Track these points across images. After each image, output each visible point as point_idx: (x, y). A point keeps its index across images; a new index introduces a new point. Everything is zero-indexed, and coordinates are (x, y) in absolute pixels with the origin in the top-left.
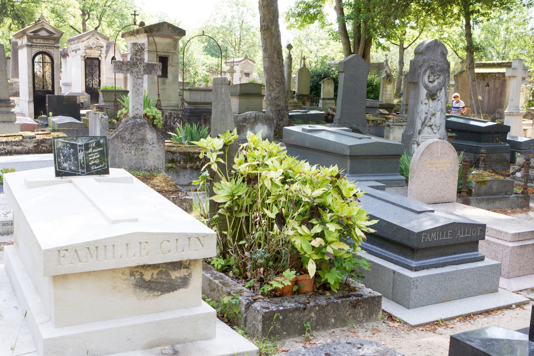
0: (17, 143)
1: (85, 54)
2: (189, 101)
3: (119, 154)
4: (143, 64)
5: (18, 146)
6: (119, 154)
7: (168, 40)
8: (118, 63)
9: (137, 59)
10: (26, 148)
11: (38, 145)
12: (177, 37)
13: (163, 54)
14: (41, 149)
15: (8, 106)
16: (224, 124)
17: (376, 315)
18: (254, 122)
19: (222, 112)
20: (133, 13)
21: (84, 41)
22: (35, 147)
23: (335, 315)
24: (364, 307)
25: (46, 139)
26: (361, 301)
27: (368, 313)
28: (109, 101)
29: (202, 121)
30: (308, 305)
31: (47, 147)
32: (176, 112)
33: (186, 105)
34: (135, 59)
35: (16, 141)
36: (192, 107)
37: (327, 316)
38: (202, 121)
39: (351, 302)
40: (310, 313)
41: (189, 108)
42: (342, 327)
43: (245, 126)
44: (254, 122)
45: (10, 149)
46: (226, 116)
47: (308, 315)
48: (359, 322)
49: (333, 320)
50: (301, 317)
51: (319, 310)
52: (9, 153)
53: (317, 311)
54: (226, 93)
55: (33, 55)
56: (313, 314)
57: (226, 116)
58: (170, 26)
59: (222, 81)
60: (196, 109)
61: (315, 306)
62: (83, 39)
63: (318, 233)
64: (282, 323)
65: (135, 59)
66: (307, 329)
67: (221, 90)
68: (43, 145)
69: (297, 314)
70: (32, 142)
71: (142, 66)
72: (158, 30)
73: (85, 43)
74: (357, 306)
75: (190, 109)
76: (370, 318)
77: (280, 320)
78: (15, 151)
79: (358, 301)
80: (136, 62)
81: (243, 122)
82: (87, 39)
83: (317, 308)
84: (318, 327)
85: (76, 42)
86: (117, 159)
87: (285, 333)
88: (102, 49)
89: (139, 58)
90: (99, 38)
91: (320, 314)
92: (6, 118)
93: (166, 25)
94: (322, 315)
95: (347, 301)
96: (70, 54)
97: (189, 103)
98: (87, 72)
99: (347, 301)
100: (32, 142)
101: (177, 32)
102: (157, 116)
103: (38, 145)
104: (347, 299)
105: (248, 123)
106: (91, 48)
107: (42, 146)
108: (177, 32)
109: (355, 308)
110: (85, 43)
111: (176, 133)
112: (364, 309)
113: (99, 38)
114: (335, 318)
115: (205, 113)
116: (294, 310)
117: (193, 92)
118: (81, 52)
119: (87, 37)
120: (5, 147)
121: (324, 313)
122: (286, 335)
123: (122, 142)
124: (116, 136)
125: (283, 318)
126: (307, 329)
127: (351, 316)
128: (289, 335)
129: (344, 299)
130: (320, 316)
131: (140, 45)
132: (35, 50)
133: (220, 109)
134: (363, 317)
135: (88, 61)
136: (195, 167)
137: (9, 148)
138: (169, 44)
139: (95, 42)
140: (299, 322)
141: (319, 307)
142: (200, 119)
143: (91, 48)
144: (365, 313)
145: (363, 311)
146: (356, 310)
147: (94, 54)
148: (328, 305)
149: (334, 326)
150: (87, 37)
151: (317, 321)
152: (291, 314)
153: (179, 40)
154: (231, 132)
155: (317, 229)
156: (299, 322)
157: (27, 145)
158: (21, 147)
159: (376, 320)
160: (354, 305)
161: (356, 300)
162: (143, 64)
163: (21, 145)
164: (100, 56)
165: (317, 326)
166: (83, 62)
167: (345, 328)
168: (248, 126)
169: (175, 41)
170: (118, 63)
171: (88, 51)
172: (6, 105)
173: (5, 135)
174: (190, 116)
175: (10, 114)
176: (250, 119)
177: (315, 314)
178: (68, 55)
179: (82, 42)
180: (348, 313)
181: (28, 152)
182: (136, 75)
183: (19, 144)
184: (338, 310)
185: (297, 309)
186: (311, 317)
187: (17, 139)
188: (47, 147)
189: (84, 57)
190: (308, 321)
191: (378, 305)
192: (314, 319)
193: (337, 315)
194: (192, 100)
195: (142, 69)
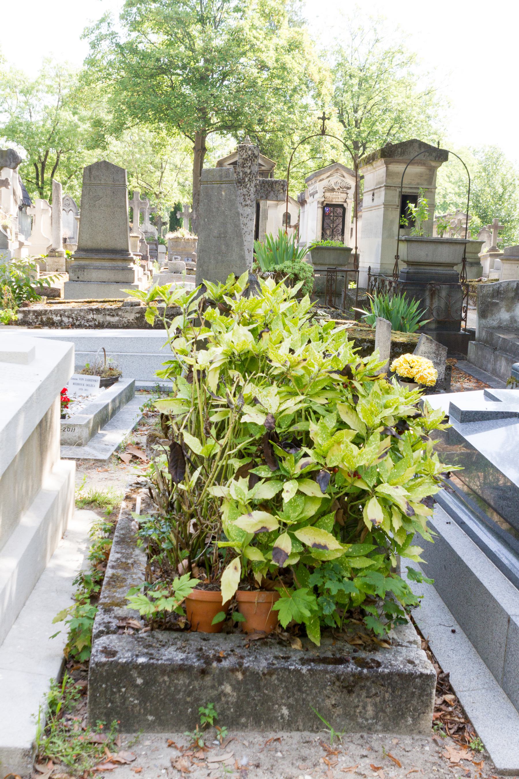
0: (112, 313)
1: (323, 199)
4: (254, 182)
5: (113, 316)
9: (245, 173)
10: (125, 320)
12: (433, 164)
15: (125, 260)
16: (223, 262)
17: (413, 719)
18: (513, 298)
19: (219, 237)
20: (321, 115)
21: (323, 179)
22: (137, 318)
23: (291, 701)
24: (376, 694)
26: (367, 678)
27: (388, 710)
28: (321, 264)
29: (427, 293)
30: (215, 664)
34: (241, 174)
35: (111, 309)
36: (412, 270)
37: (266, 699)
38: (427, 293)
39: (338, 677)
40: (220, 684)
42: (312, 731)
43: (497, 304)
44: (513, 298)
45: (101, 320)
47: (213, 687)
48: (362, 727)
49: (285, 711)
50: (194, 689)
51: (244, 682)
52: (100, 326)
53: (238, 682)
54: (230, 201)
56: (228, 689)
57: (227, 245)
59: (221, 176)
60: (418, 273)
61: (233, 670)
62: (322, 177)
63: (267, 501)
64: (144, 695)
65: (241, 174)
66: (203, 720)
69: (182, 680)
70: (134, 312)
71: (253, 185)
72: (403, 153)
73: (325, 183)
74: (357, 689)
75: (408, 273)
76: (397, 724)
77: (137, 686)
78: (109, 323)
79: (360, 677)
80: (244, 179)
81: (493, 297)
82: (328, 177)
83: (240, 676)
84: (243, 720)
85: (313, 181)
87: (150, 718)
88: (348, 191)
89: (249, 171)
90: (345, 174)
91: (247, 691)
92: (120, 276)
93: (416, 145)
94: (252, 693)
95: (326, 672)
96: (308, 201)
97: (409, 263)
98: (325, 225)
99: (326, 672)
100: (134, 312)
101: (434, 154)
102: (301, 276)
104: (330, 667)
105: (502, 300)
106: (333, 190)
108: (434, 154)
109: (350, 692)
110: (325, 183)
112: (378, 699)
113: (345, 174)
114: (290, 707)
115: (434, 279)
116: (173, 671)
117: (414, 245)
118: (319, 197)
119: (328, 174)
120: (95, 317)
121: (259, 689)
122: (154, 722)
125: (146, 683)
126: (203, 720)
127: (339, 711)
128: (162, 724)
129: (321, 667)
130: (248, 696)
131: (250, 149)
133: (216, 232)
134: (376, 717)
135: (327, 209)
137: (100, 318)
138: (421, 175)
139: (339, 181)
140: (188, 699)
141: (244, 673)
142: (423, 291)
143: (333, 190)
144: (379, 710)
145: (375, 705)
146: (354, 699)
147: (337, 198)
148: (270, 674)
149: (289, 725)
150: (328, 174)
151: (238, 706)
152: (166, 678)
153: (437, 167)
154: (237, 278)
155: (265, 491)
156: (188, 699)
157: (126, 315)
158: (116, 319)
159: (414, 730)
160: (349, 686)
161: (354, 675)
162: (254, 182)
163: (117, 315)
164: (345, 202)
165: (240, 716)
166: (320, 211)
167: (316, 737)
168: (503, 304)
169: (430, 170)
171: (328, 194)
172: (122, 257)
173: (86, 300)
174: (405, 284)
175: (126, 272)
176: (506, 291)
177: (234, 688)
178: (306, 201)
179: (321, 180)
180: (328, 703)
181: (128, 326)
182: (242, 201)
183: (114, 313)
184: (299, 690)
185: (183, 669)
186: (223, 694)
187: (114, 306)
189: (323, 203)
190: (212, 700)
191: (421, 695)
192: (233, 699)
193: (297, 700)
195: (253, 190)
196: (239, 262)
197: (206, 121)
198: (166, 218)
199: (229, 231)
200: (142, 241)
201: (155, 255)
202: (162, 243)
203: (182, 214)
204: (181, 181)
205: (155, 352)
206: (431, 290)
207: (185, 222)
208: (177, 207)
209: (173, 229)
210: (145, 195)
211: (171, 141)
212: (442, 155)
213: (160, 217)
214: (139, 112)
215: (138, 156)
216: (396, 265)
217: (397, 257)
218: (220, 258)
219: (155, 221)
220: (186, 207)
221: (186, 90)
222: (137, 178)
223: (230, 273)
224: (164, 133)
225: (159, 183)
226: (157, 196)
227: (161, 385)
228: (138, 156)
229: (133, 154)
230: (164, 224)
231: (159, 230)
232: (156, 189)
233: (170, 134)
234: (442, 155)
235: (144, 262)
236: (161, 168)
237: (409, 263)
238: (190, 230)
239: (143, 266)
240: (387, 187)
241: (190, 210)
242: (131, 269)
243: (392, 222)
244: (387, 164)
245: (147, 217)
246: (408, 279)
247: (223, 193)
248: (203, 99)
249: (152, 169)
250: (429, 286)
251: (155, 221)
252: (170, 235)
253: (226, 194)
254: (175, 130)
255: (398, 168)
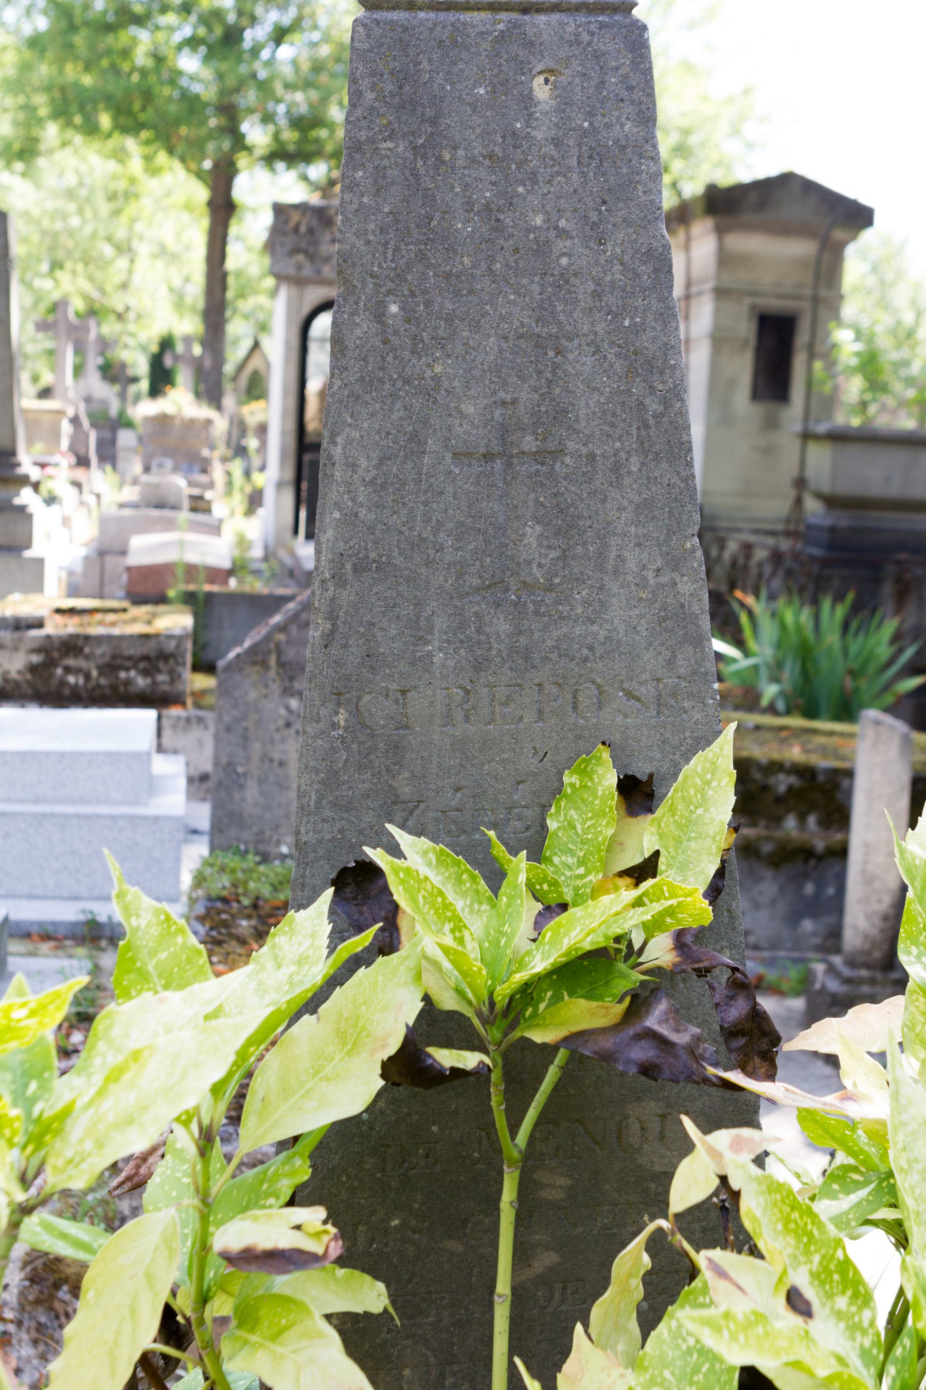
2: (826, 487)
3: (266, 758)
6: (266, 758)
7: (801, 248)
8: (295, 217)
11: (50, 664)
13: (774, 304)
14: (63, 683)
19: (498, 454)
22: (33, 669)
25: (87, 638)
31: (87, 676)
32: (770, 541)
33: (813, 507)
36: (843, 520)
41: (828, 522)
46: (564, 524)
55: (306, 309)
57: (564, 524)
58: (809, 187)
67: (510, 90)
68: (70, 662)
70: (24, 647)
75: (832, 530)
86: (251, 793)
97: (832, 502)
100: (24, 647)
103: (50, 664)
107: (68, 670)
111: (739, 643)
117: (852, 451)
123: (288, 692)
124: (253, 651)
132: (315, 295)
133: (471, 417)
136: (767, 848)
142: (877, 581)
154: (637, 794)
170: (295, 217)
174: (825, 563)
188: (87, 676)
194: (848, 487)
196: (651, 660)
197: (239, 142)
198: (141, 366)
199: (586, 406)
200: (75, 421)
201: (108, 454)
202: (129, 424)
203: (176, 358)
204: (177, 282)
205: (83, 801)
206: (899, 580)
207: (183, 377)
208: (166, 344)
209: (155, 391)
210: (93, 312)
211: (151, 186)
212: (858, 217)
213: (123, 366)
214: (74, 108)
215: (75, 221)
216: (799, 502)
217: (800, 483)
218: (502, 625)
219: (113, 372)
220: (188, 340)
221: (189, 63)
222: (74, 273)
223: (576, 753)
224: (136, 165)
225: (124, 286)
226: (120, 317)
227: (103, 918)
228: (75, 221)
229: (65, 217)
230: (135, 380)
231: (122, 396)
232: (117, 302)
233: (153, 171)
234: (858, 217)
235: (80, 474)
236: (124, 249)
237: (832, 502)
238: (198, 395)
239: (77, 485)
240: (721, 293)
241: (197, 350)
242: (22, 509)
243: (731, 384)
244: (720, 231)
245: (94, 361)
246: (832, 546)
247: (541, 90)
248: (231, 81)
249: (108, 250)
250: (890, 569)
251: (113, 372)
252: (146, 409)
253: (564, 101)
254: (162, 157)
255: (748, 243)
